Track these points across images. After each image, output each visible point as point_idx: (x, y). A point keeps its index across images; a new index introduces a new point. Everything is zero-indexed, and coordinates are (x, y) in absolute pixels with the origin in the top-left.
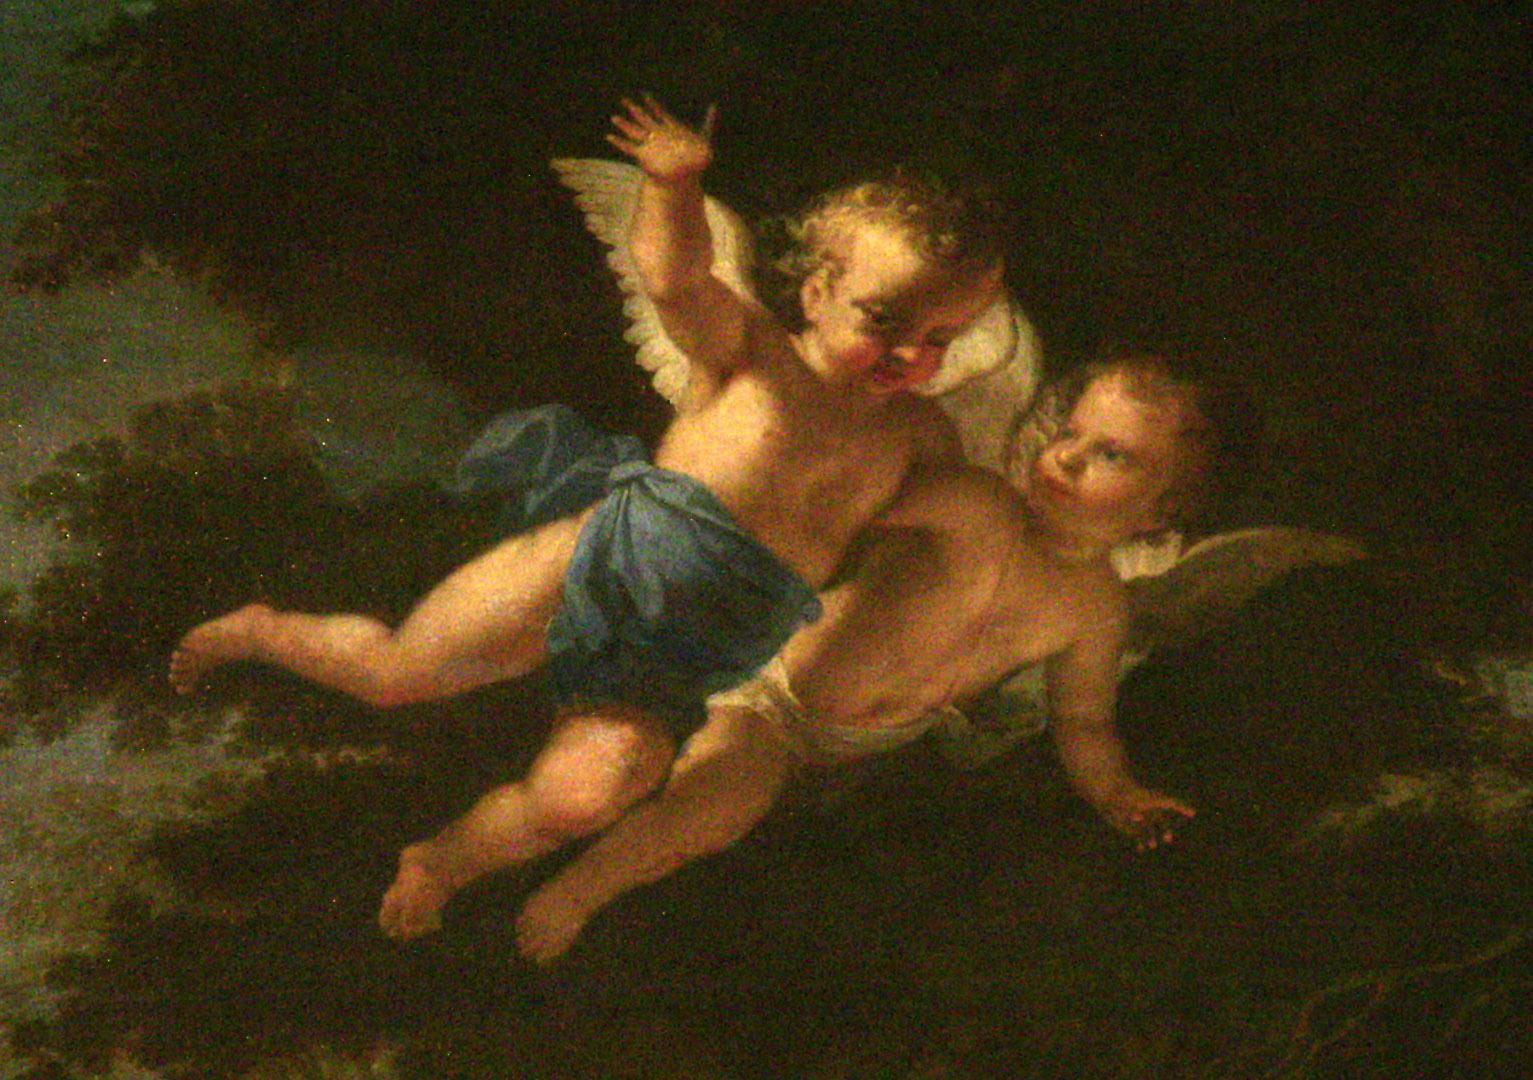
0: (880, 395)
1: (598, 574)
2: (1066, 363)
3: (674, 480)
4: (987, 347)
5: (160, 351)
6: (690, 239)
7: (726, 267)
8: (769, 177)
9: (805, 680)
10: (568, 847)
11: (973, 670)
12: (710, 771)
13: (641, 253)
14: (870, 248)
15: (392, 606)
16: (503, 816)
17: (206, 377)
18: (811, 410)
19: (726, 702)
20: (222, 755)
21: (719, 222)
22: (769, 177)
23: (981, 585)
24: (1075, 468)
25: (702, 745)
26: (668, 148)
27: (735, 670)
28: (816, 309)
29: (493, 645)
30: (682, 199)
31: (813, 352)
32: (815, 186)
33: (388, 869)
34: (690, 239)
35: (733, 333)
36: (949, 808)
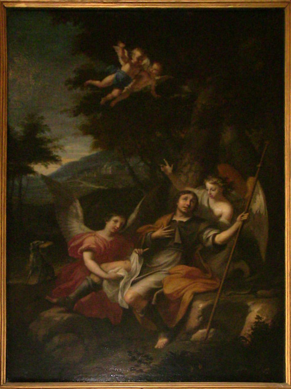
0: (97, 275)
1: (117, 78)
2: (152, 62)
3: (122, 71)
4: (146, 61)
5: (82, 60)
6: (123, 52)
7: (126, 54)
8: (130, 47)
9: (132, 86)
10: (114, 98)
11: (144, 86)
12: (125, 93)
13: (120, 54)
14: (137, 53)
15: (101, 80)
16: (109, 96)
17: (12, 70)
18: (132, 66)
19: (126, 88)
20: (88, 91)
21: (126, 51)
22: (130, 47)
23: (145, 79)
24: (152, 71)
25: (124, 91)
26: (122, 45)
27: (126, 85)
28: (133, 58)
29: (109, 83)
30: (123, 49)
31: (133, 61)
32: (133, 49)
33: (100, 100)
34: (123, 52)
35: (127, 60)
36: (142, 96)
